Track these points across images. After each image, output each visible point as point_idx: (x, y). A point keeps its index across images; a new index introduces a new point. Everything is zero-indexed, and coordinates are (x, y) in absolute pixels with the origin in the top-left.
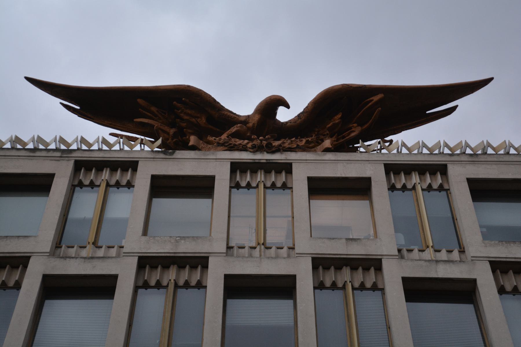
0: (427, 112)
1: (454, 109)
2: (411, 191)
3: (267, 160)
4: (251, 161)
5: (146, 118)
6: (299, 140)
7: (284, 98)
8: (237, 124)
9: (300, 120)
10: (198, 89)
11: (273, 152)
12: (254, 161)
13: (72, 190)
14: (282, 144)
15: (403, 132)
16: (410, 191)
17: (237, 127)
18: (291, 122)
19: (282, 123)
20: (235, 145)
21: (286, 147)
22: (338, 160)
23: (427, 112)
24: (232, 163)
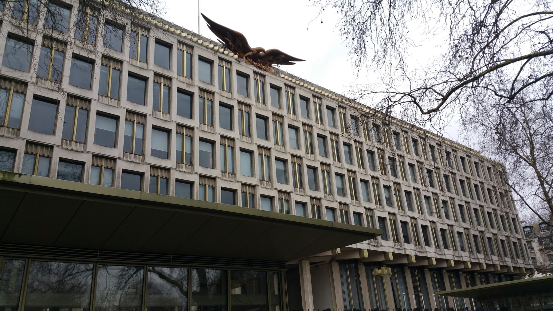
1: (294, 63)
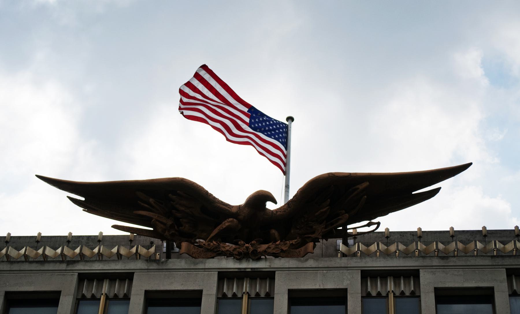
0: (413, 193)
2: (386, 298)
3: (252, 268)
4: (236, 270)
5: (144, 210)
6: (284, 244)
7: (271, 194)
8: (228, 218)
9: (289, 209)
10: (190, 181)
11: (259, 259)
12: (240, 270)
13: (77, 304)
14: (267, 250)
15: (390, 214)
16: (385, 298)
17: (228, 221)
18: (280, 210)
19: (272, 211)
20: (222, 251)
21: (271, 253)
22: (318, 268)
23: (413, 193)
24: (219, 273)
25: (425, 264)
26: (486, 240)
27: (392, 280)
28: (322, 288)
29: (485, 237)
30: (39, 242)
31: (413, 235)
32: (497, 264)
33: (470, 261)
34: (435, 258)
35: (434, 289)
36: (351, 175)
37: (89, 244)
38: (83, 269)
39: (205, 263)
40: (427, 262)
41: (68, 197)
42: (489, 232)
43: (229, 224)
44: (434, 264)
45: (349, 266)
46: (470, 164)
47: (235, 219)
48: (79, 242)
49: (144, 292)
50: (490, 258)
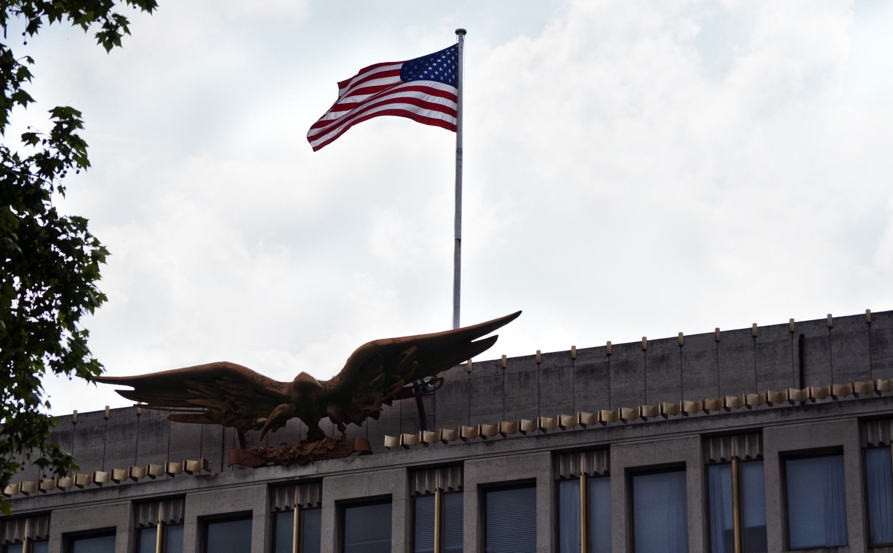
0: (472, 341)
3: (300, 477)
4: (285, 480)
8: (281, 403)
24: (269, 484)
25: (470, 454)
26: (575, 364)
27: (440, 474)
28: (367, 495)
29: (574, 361)
30: (108, 418)
31: (497, 366)
32: (542, 447)
33: (515, 445)
34: (481, 444)
35: (476, 486)
36: (396, 342)
37: (160, 416)
38: (135, 495)
39: (254, 474)
40: (473, 451)
41: (117, 391)
42: (579, 353)
43: (280, 411)
44: (479, 452)
45: (395, 463)
46: (520, 312)
47: (286, 403)
48: (149, 413)
49: (196, 518)
50: (535, 439)
